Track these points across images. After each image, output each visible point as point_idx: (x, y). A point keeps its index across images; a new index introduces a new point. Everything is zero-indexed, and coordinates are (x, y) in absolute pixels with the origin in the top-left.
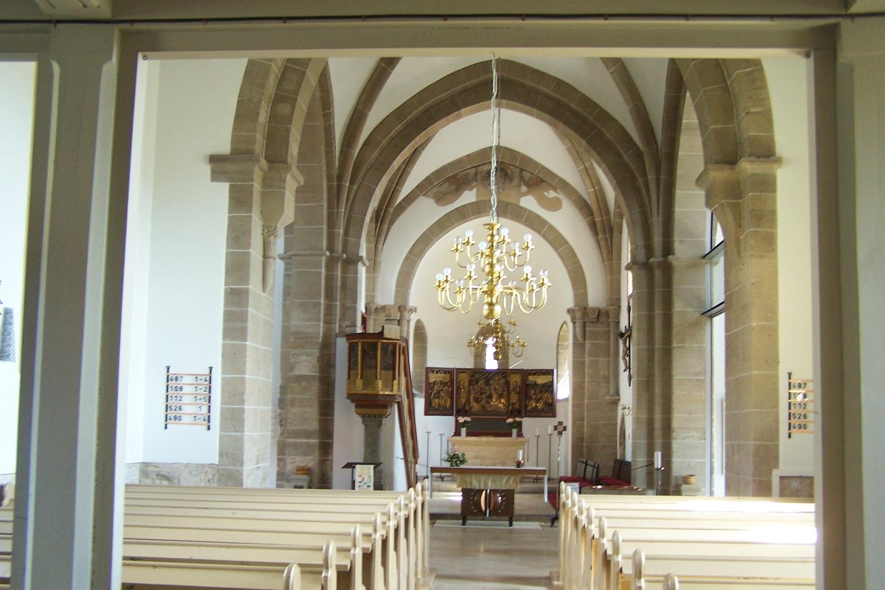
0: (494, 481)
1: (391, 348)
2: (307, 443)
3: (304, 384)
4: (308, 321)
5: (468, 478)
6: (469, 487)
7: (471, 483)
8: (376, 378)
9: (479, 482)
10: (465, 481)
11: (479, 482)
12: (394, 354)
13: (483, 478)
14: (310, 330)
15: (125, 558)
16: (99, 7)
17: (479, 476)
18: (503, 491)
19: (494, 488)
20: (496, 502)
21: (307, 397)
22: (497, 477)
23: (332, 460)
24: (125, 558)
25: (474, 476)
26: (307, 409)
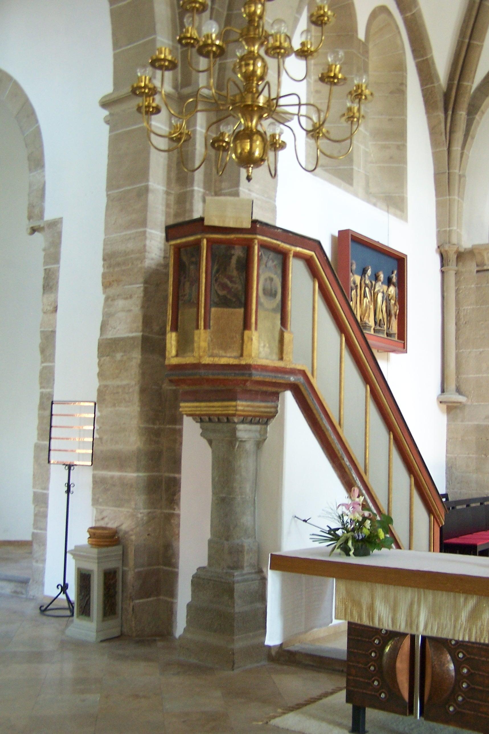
0: (435, 612)
1: (238, 252)
2: (120, 478)
3: (119, 356)
4: (128, 228)
5: (364, 591)
6: (366, 621)
7: (371, 608)
8: (197, 328)
9: (394, 609)
10: (358, 604)
11: (394, 609)
12: (245, 266)
13: (406, 596)
14: (130, 246)
15: (430, 550)
16: (454, 244)
17: (393, 591)
18: (461, 645)
19: (433, 632)
20: (439, 678)
21: (125, 382)
22: (444, 598)
23: (178, 516)
24: (430, 550)
25: (380, 590)
26: (123, 409)
